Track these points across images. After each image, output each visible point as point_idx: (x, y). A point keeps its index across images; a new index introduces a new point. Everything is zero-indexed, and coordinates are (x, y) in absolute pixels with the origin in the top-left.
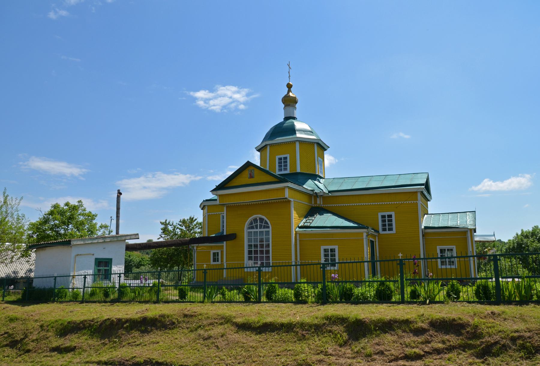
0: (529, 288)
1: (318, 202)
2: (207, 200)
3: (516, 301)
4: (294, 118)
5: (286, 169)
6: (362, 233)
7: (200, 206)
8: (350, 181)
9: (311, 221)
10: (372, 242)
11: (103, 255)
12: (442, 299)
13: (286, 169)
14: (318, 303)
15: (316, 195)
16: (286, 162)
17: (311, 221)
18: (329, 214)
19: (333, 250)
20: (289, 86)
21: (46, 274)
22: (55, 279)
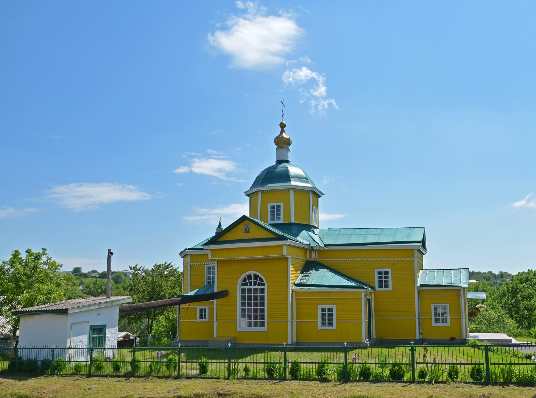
0: (510, 372)
1: (314, 256)
2: (189, 249)
3: (500, 382)
4: (287, 162)
5: (279, 219)
6: (361, 293)
7: (180, 254)
8: (346, 232)
9: (307, 278)
10: (369, 300)
11: (97, 322)
12: (444, 380)
13: (279, 219)
14: (340, 381)
15: (312, 249)
16: (279, 211)
17: (307, 278)
18: (326, 270)
19: (330, 310)
20: (283, 126)
21: (40, 345)
22: (53, 351)
